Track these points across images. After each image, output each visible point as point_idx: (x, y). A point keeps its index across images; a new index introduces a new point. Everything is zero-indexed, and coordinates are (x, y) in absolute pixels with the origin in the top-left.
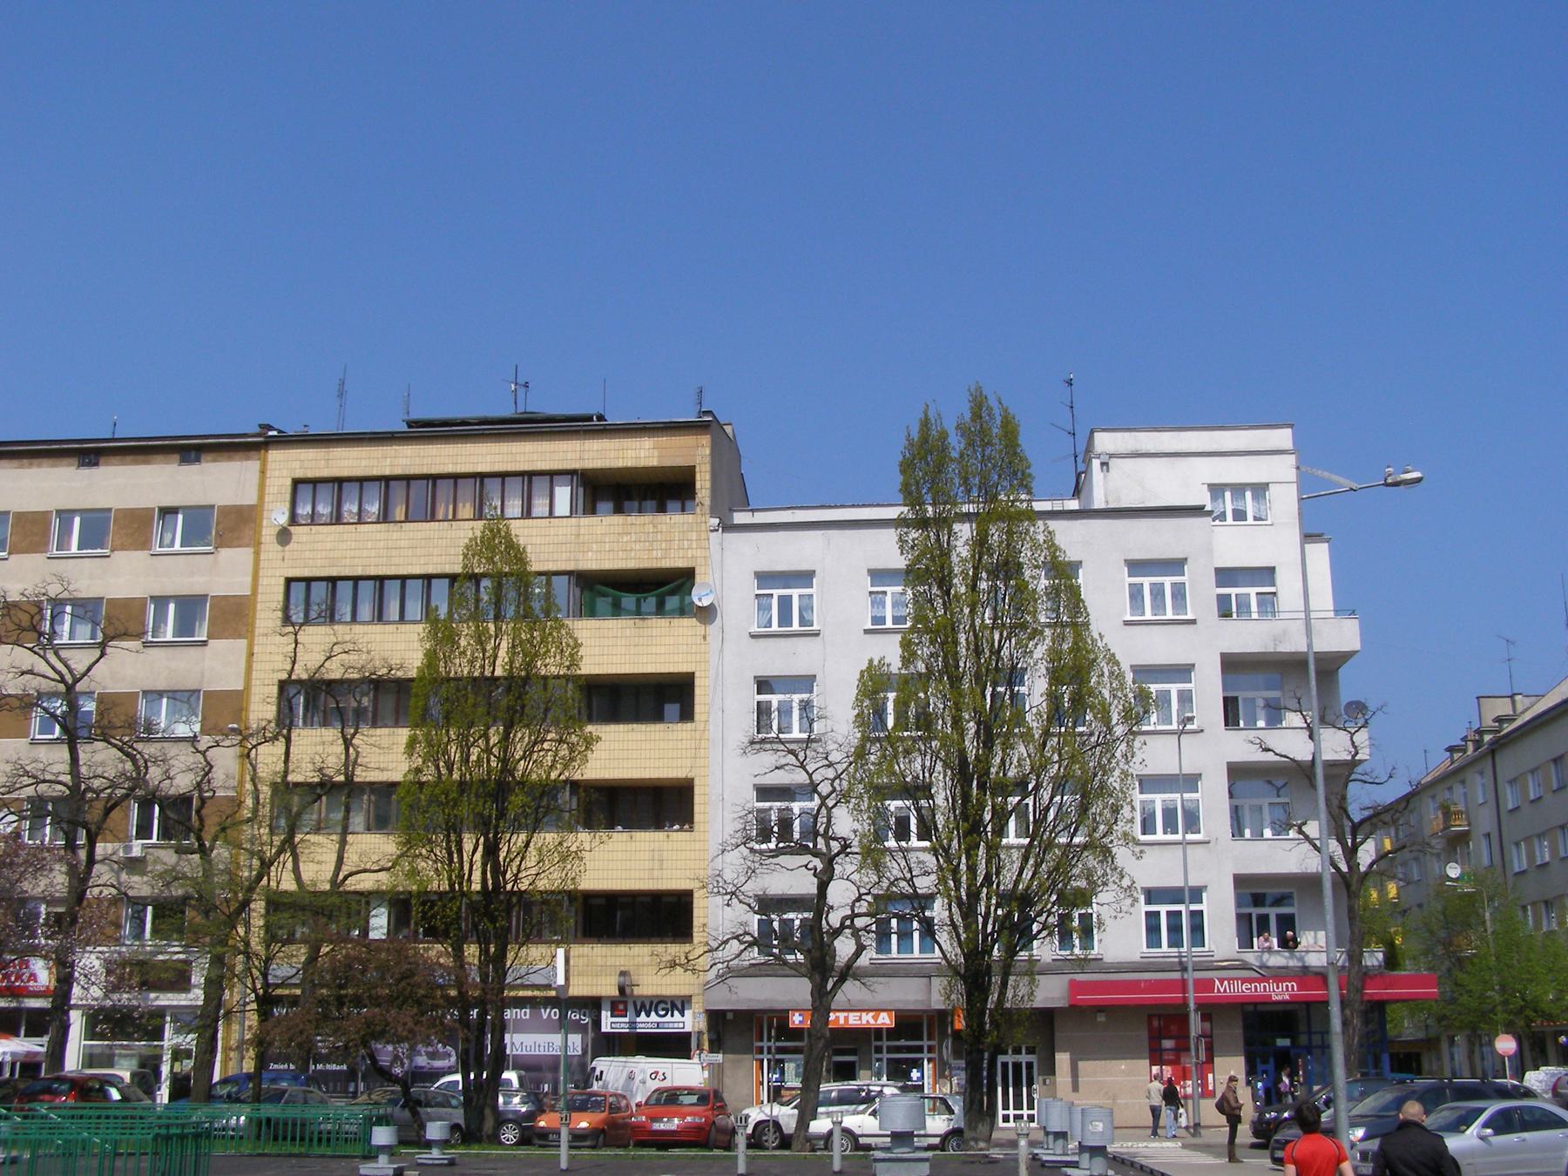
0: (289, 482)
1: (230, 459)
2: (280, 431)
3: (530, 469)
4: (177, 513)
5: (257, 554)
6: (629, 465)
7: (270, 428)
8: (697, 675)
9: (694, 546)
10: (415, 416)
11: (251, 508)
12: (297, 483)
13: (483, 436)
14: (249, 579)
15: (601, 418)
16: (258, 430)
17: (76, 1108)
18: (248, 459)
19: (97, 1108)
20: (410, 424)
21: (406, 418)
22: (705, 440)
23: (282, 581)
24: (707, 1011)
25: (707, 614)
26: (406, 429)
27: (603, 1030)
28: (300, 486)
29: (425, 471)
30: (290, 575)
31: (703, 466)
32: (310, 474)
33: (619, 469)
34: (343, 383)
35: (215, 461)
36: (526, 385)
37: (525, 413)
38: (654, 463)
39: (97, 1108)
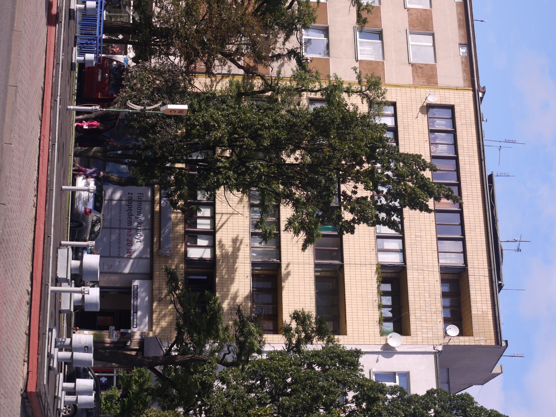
0: (452, 103)
1: (464, 71)
2: (482, 98)
6: (472, 297)
7: (484, 93)
9: (424, 336)
10: (496, 180)
12: (452, 108)
15: (501, 287)
16: (482, 86)
17: (100, 21)
19: (100, 27)
20: (491, 177)
21: (495, 174)
25: (352, 68)
26: (488, 174)
29: (462, 179)
30: (397, 105)
32: (457, 115)
35: (462, 63)
36: (519, 250)
37: (502, 251)
38: (474, 311)
39: (100, 27)
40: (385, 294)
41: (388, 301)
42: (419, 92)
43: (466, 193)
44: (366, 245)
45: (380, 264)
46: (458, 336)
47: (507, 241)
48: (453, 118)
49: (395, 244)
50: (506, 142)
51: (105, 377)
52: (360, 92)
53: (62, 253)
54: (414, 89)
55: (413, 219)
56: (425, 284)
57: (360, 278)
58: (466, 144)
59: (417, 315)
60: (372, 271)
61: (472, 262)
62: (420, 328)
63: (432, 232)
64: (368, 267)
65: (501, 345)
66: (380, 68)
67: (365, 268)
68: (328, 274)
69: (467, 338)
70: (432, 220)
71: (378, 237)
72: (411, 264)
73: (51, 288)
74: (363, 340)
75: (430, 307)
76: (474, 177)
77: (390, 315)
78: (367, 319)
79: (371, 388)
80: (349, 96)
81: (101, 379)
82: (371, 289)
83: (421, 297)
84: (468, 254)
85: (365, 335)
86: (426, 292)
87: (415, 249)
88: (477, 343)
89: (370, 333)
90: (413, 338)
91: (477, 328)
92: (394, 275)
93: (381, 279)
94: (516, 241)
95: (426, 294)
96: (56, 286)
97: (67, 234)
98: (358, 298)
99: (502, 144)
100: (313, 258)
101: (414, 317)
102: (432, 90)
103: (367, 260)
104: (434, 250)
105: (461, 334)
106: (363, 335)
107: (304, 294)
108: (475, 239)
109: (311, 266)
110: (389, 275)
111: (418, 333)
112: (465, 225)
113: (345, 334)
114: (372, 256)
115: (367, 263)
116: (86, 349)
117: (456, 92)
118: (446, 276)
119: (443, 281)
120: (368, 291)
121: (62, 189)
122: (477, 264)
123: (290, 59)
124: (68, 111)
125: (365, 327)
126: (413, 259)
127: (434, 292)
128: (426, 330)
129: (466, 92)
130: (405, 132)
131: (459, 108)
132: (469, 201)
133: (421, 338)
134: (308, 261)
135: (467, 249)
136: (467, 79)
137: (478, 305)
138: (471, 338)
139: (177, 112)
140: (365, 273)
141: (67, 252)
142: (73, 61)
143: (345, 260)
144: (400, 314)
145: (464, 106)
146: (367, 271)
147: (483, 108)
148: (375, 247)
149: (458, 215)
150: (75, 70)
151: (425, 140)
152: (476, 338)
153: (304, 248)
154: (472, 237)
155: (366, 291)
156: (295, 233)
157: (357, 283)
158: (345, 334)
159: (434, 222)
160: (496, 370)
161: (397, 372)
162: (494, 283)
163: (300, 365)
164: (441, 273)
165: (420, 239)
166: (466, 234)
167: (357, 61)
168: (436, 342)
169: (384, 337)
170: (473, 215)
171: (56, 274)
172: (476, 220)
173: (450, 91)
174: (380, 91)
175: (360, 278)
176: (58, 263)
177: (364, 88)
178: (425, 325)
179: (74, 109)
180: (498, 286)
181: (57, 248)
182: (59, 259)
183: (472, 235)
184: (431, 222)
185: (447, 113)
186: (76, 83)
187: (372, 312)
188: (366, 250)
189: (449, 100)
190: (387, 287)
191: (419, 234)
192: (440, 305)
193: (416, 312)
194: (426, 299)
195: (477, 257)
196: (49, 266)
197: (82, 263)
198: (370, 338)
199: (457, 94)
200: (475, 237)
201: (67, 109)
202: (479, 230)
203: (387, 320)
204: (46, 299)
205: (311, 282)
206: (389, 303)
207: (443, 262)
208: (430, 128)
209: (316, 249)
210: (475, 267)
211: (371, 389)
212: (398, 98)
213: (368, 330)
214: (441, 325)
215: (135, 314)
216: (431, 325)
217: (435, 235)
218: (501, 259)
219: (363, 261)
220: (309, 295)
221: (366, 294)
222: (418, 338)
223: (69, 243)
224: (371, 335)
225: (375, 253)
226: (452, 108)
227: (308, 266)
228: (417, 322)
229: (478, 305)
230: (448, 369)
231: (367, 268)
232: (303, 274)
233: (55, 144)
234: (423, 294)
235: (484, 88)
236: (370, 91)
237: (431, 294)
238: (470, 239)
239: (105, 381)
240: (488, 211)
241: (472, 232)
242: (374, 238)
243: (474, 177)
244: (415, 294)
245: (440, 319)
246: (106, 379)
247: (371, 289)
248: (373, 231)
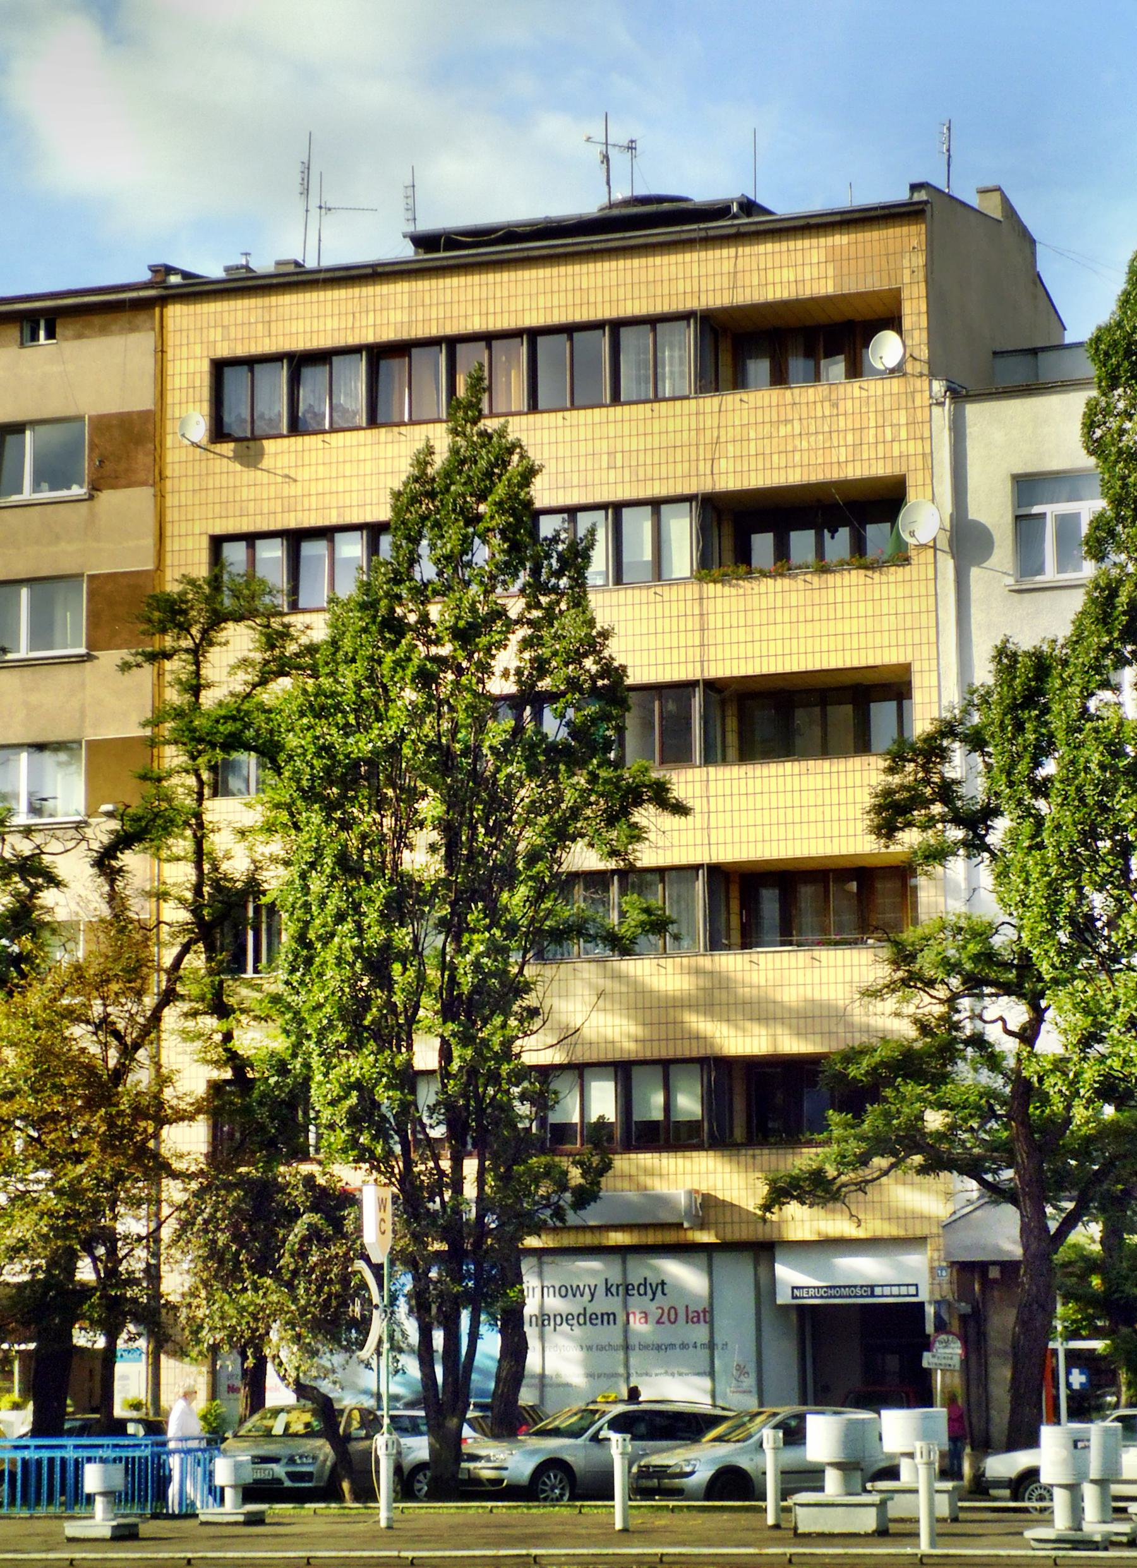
0: (206, 366)
1: (104, 331)
2: (186, 275)
3: (614, 315)
4: (23, 432)
5: (160, 497)
7: (169, 270)
8: (916, 667)
9: (903, 435)
11: (145, 415)
12: (219, 367)
13: (875, 209)
14: (149, 542)
15: (749, 207)
16: (147, 276)
18: (133, 330)
20: (425, 242)
21: (410, 228)
22: (912, 235)
23: (205, 543)
24: (953, 1264)
26: (407, 251)
27: (780, 1301)
28: (228, 372)
29: (434, 331)
31: (915, 288)
32: (240, 351)
33: (785, 304)
34: (307, 168)
35: (79, 336)
36: (631, 147)
38: (827, 288)
39: (116, 1446)
40: (782, 552)
41: (802, 541)
42: (176, 466)
43: (477, 319)
44: (644, 615)
45: (698, 571)
46: (899, 331)
47: (608, 183)
48: (250, 362)
49: (637, 524)
50: (306, 192)
51: (1068, 1373)
52: (197, 653)
53: (807, 1521)
54: (168, 483)
55: (561, 477)
56: (752, 435)
57: (742, 630)
58: (329, 320)
59: (843, 459)
60: (719, 594)
61: (681, 297)
62: (881, 447)
63: (597, 419)
64: (709, 606)
65: (926, 202)
66: (109, 588)
67: (711, 617)
68: (732, 724)
69: (907, 308)
70: (560, 422)
71: (618, 580)
72: (694, 480)
73: (924, 1546)
74: (924, 616)
75: (819, 422)
76: (427, 295)
77: (844, 533)
78: (862, 604)
79: (1105, 619)
80: (209, 686)
81: (1076, 1386)
82: (771, 596)
83: (790, 448)
84: (659, 310)
85: (908, 610)
86: (775, 434)
87: (649, 468)
88: (921, 275)
89: (900, 594)
90: (912, 467)
91: (877, 276)
92: (728, 530)
93: (742, 569)
94: (606, 158)
95: (782, 433)
96: (917, 1535)
97: (596, 1507)
98: (802, 634)
99: (314, 202)
100: (690, 771)
101: (850, 465)
102: (169, 426)
103: (689, 612)
104: (649, 414)
105: (894, 322)
106: (908, 617)
107: (796, 794)
108: (614, 290)
109: (712, 776)
110: (728, 543)
111: (896, 453)
112: (570, 319)
113: (906, 668)
114: (674, 598)
115: (697, 612)
116: (1080, 1445)
117: (170, 355)
118: (726, 372)
119: (739, 382)
120: (779, 604)
121: (625, 1530)
122: (688, 281)
123: (120, 870)
124: (395, 1525)
125: (885, 611)
126: (679, 473)
127: (774, 410)
128: (888, 430)
129: (170, 324)
130: (299, 507)
131: (219, 345)
132: (498, 310)
133: (912, 443)
134: (697, 785)
135: (644, 312)
136: (130, 322)
137: (807, 276)
138: (905, 294)
139: (382, 1215)
140: (727, 616)
141: (805, 1509)
142: (241, 1518)
143: (691, 677)
144: (836, 505)
145: (212, 330)
146: (719, 609)
147: (213, 269)
148: (649, 587)
149: (541, 341)
150: (263, 1513)
151: (321, 445)
152: (907, 280)
153: (680, 809)
154: (607, 298)
155: (779, 612)
156: (638, 839)
157: (757, 637)
158: (906, 668)
159: (567, 414)
160: (992, 207)
161: (1014, 510)
162: (743, 229)
163: (1039, 821)
164: (717, 390)
165: (619, 456)
166: (600, 316)
167: (87, 658)
168: (922, 399)
169: (912, 553)
170: (541, 298)
171: (867, 1535)
172: (555, 288)
173: (170, 372)
174: (190, 596)
175: (742, 630)
176: (836, 1531)
177: (186, 643)
178: (872, 431)
179: (390, 1509)
180: (749, 215)
181: (796, 1534)
182: (826, 1530)
183: (600, 299)
184: (567, 423)
185: (235, 379)
186: (323, 1505)
187: (839, 591)
188: (659, 614)
189: (198, 376)
190: (763, 544)
191: (605, 457)
192: (811, 391)
193: (835, 460)
194: (797, 431)
195: (666, 284)
196: (872, 1555)
197: (831, 1464)
198: (915, 593)
199: (178, 351)
200: (607, 291)
201: (389, 1527)
202: (584, 278)
203: (859, 546)
204: (958, 1560)
205: (758, 773)
206: (809, 535)
207: (686, 384)
208: (285, 432)
209: (663, 762)
210: (696, 289)
211: (1105, 623)
212: (197, 531)
213: (893, 602)
214: (871, 387)
215: (878, 1291)
216: (872, 416)
217: (604, 410)
218: (666, 206)
219: (693, 623)
220: (796, 778)
221: (787, 611)
222: (912, 451)
223: (770, 1503)
224: (907, 594)
225: (666, 588)
226: (219, 367)
227: (712, 785)
228: (865, 456)
229: (807, 276)
230: (995, 353)
231: (711, 610)
232: (736, 798)
233: (535, 1557)
234: (783, 441)
235: (154, 269)
236: (191, 625)
237: (782, 418)
238: (614, 304)
239: (1081, 1373)
240: (525, 254)
241: (592, 300)
242: (622, 593)
243: (427, 295)
244: (783, 464)
245: (855, 388)
246: (1075, 1371)
247: (771, 596)
248: (600, 596)
